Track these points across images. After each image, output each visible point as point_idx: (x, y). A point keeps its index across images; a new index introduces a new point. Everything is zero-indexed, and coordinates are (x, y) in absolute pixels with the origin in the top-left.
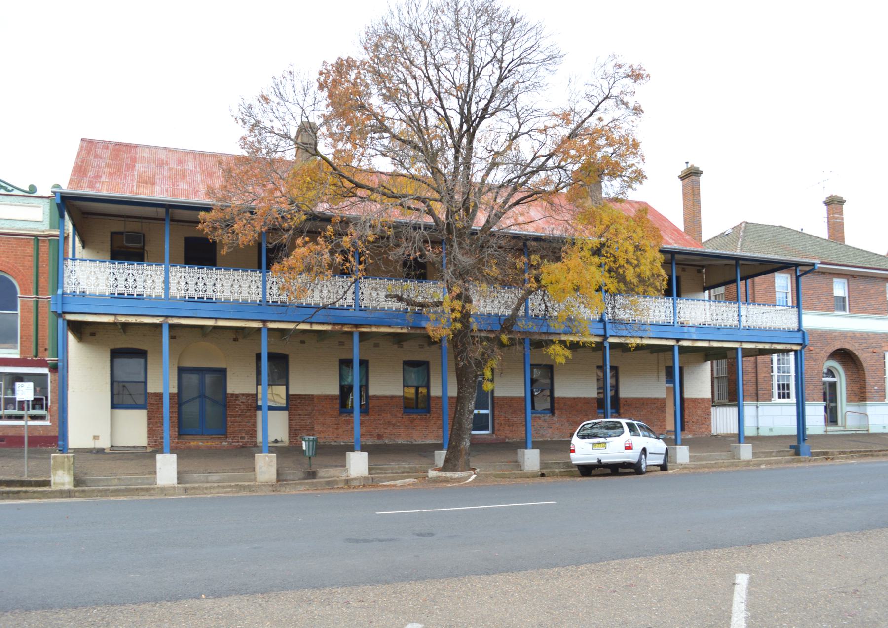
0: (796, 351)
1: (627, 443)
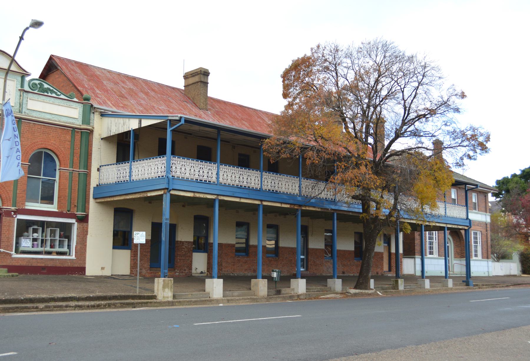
0: (465, 230)
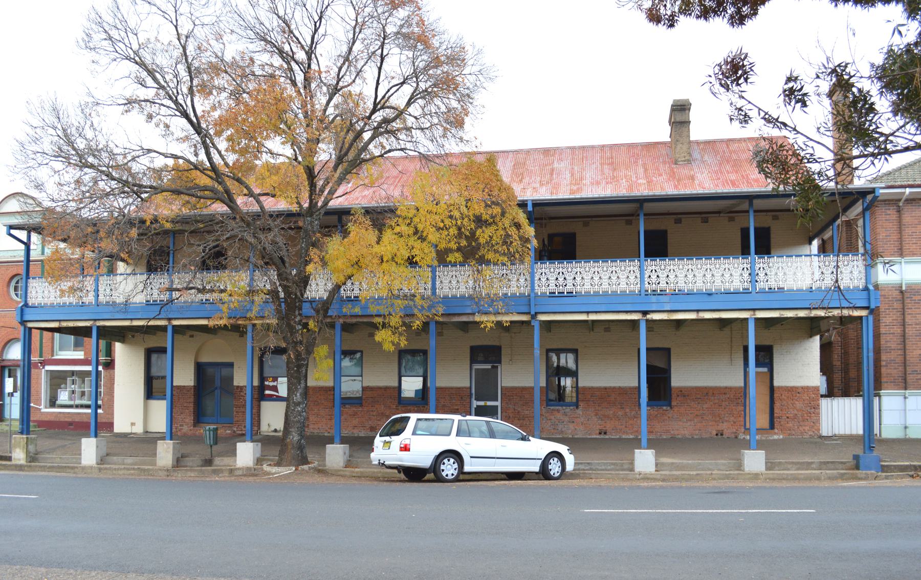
1: (403, 442)
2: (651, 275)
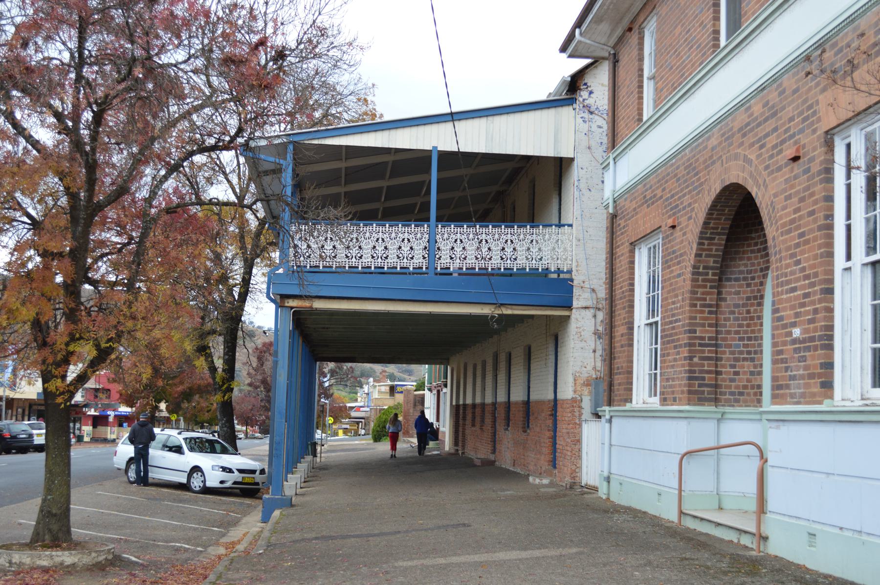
2: (377, 245)
